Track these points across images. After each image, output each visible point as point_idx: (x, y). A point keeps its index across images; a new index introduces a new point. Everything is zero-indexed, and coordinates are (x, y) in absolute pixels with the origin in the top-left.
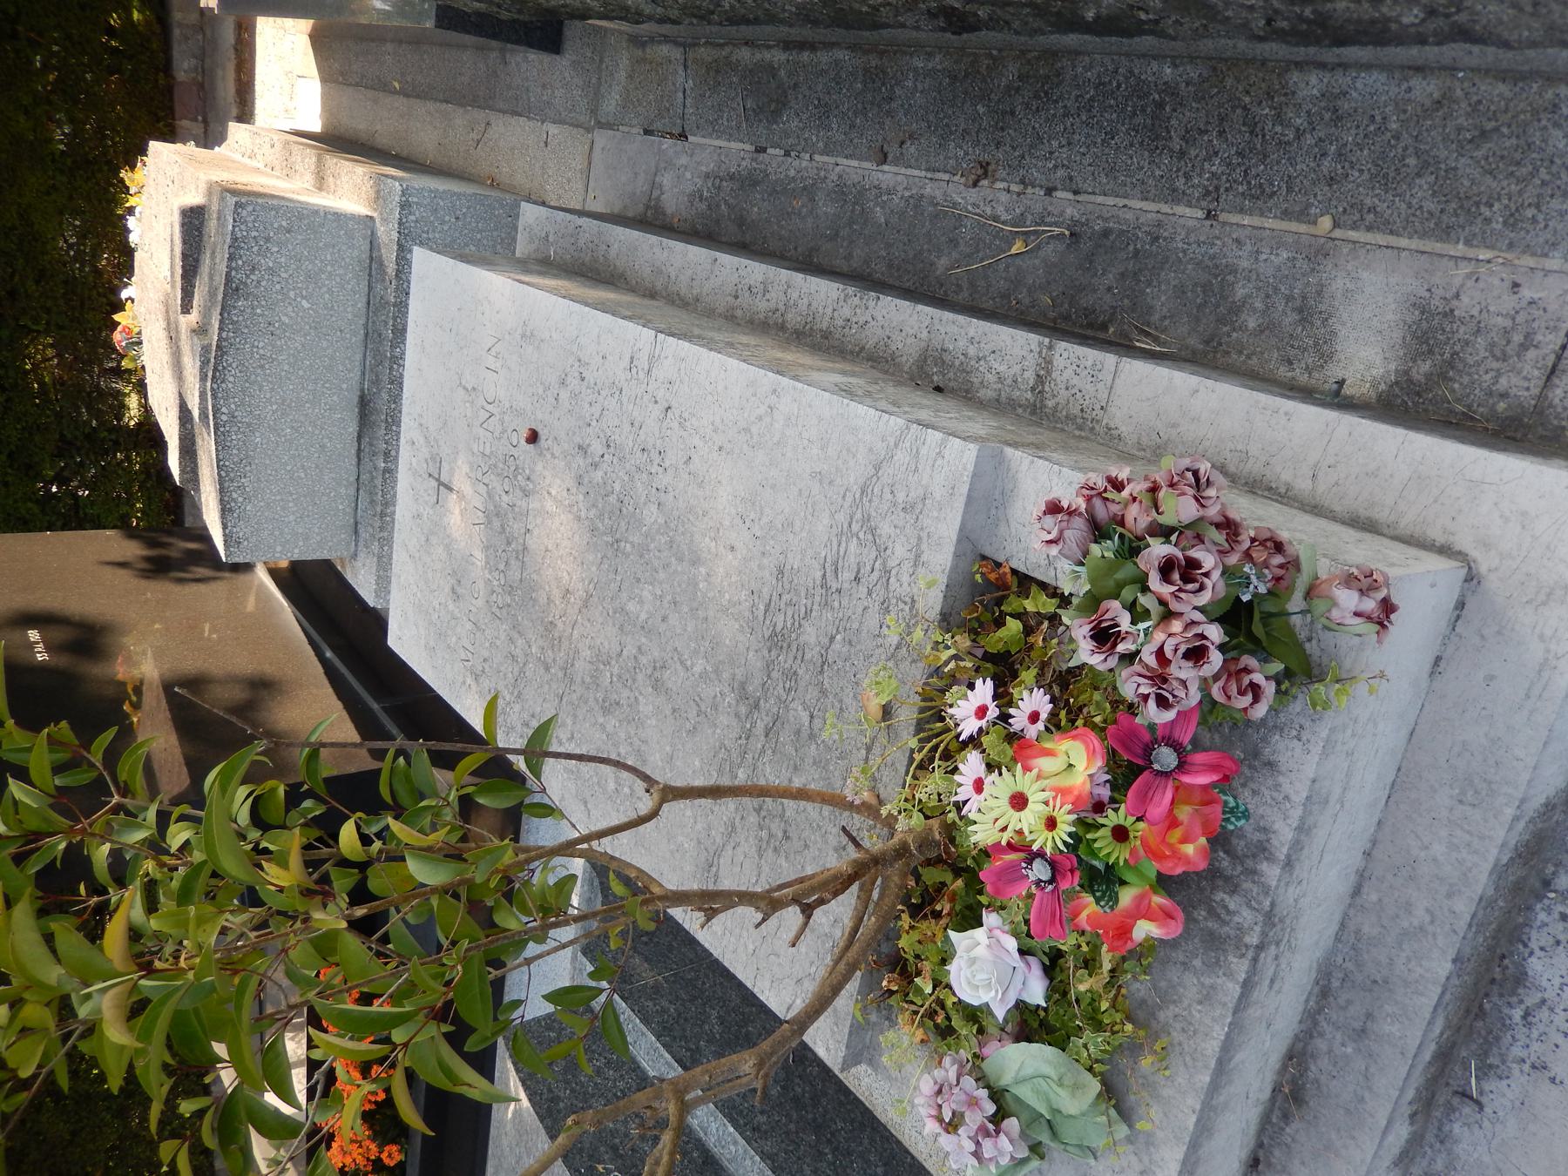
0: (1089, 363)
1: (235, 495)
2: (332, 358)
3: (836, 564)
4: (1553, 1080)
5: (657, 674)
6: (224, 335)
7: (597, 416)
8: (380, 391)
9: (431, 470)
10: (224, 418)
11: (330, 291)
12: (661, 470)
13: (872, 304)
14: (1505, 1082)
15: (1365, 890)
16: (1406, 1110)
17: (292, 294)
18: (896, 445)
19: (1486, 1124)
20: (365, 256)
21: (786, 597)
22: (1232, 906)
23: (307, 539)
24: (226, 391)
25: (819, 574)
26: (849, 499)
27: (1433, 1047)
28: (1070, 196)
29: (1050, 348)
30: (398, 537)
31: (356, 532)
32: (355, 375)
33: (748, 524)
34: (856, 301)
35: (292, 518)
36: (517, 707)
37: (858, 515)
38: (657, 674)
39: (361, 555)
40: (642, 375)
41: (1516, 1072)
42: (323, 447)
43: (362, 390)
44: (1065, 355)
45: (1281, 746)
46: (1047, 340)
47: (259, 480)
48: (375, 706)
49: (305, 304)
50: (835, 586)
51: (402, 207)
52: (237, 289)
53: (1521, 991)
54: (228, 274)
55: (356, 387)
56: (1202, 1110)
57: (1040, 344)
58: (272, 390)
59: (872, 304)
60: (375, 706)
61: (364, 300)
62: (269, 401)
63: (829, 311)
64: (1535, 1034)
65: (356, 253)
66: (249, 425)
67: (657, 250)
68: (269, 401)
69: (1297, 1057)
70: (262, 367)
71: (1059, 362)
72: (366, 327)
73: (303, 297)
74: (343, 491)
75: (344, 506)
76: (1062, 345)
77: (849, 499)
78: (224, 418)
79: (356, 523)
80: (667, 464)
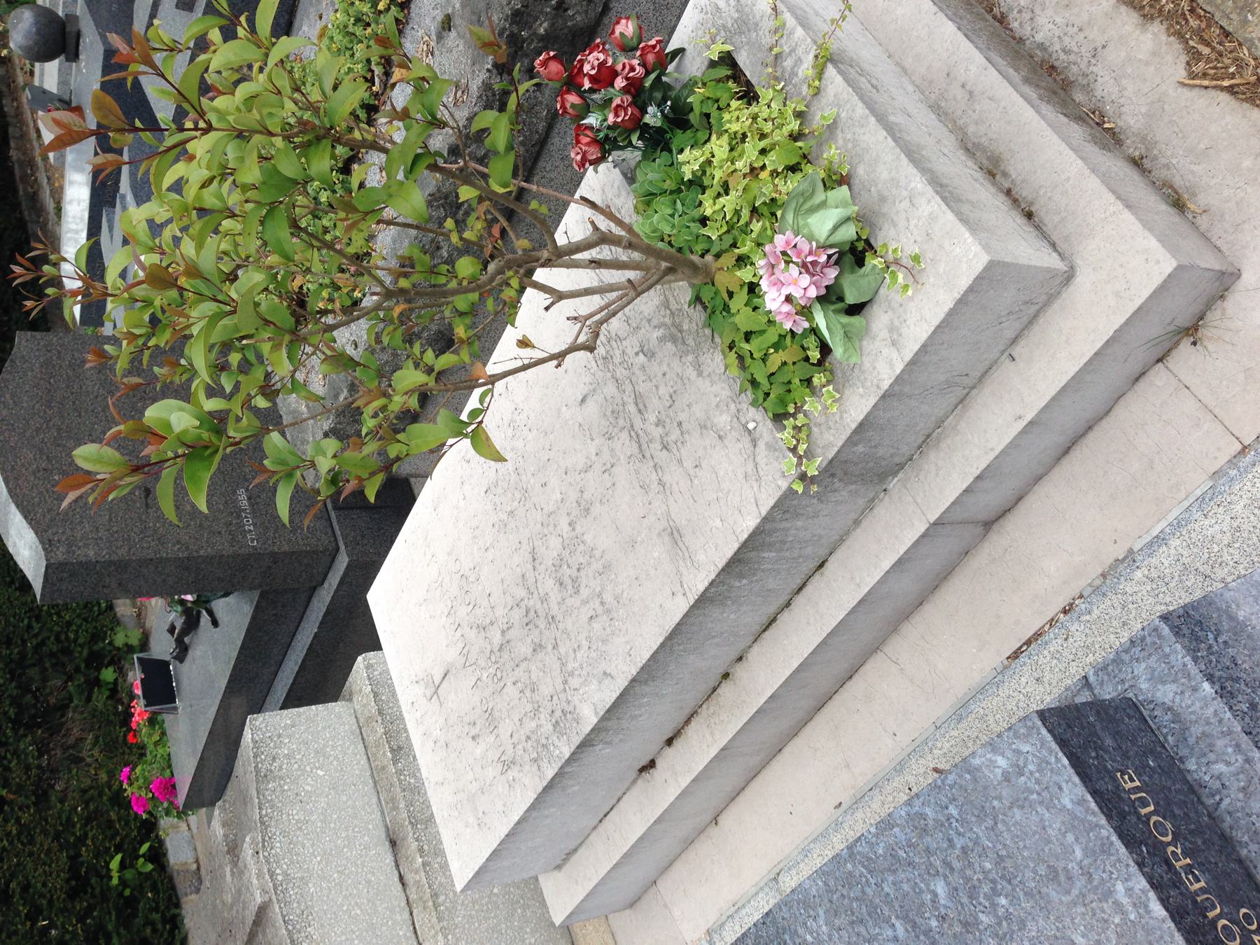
2: (354, 808)
4: (1104, 47)
10: (280, 878)
11: (336, 758)
14: (1099, 79)
17: (308, 769)
19: (1122, 101)
20: (355, 727)
24: (276, 855)
27: (1011, 71)
32: (377, 815)
41: (1095, 69)
42: (369, 882)
47: (322, 925)
49: (320, 773)
52: (266, 776)
53: (1050, 50)
54: (256, 767)
55: (381, 825)
58: (313, 845)
64: (1075, 49)
65: (347, 727)
66: (302, 878)
69: (970, 148)
70: (300, 829)
72: (373, 777)
74: (398, 917)
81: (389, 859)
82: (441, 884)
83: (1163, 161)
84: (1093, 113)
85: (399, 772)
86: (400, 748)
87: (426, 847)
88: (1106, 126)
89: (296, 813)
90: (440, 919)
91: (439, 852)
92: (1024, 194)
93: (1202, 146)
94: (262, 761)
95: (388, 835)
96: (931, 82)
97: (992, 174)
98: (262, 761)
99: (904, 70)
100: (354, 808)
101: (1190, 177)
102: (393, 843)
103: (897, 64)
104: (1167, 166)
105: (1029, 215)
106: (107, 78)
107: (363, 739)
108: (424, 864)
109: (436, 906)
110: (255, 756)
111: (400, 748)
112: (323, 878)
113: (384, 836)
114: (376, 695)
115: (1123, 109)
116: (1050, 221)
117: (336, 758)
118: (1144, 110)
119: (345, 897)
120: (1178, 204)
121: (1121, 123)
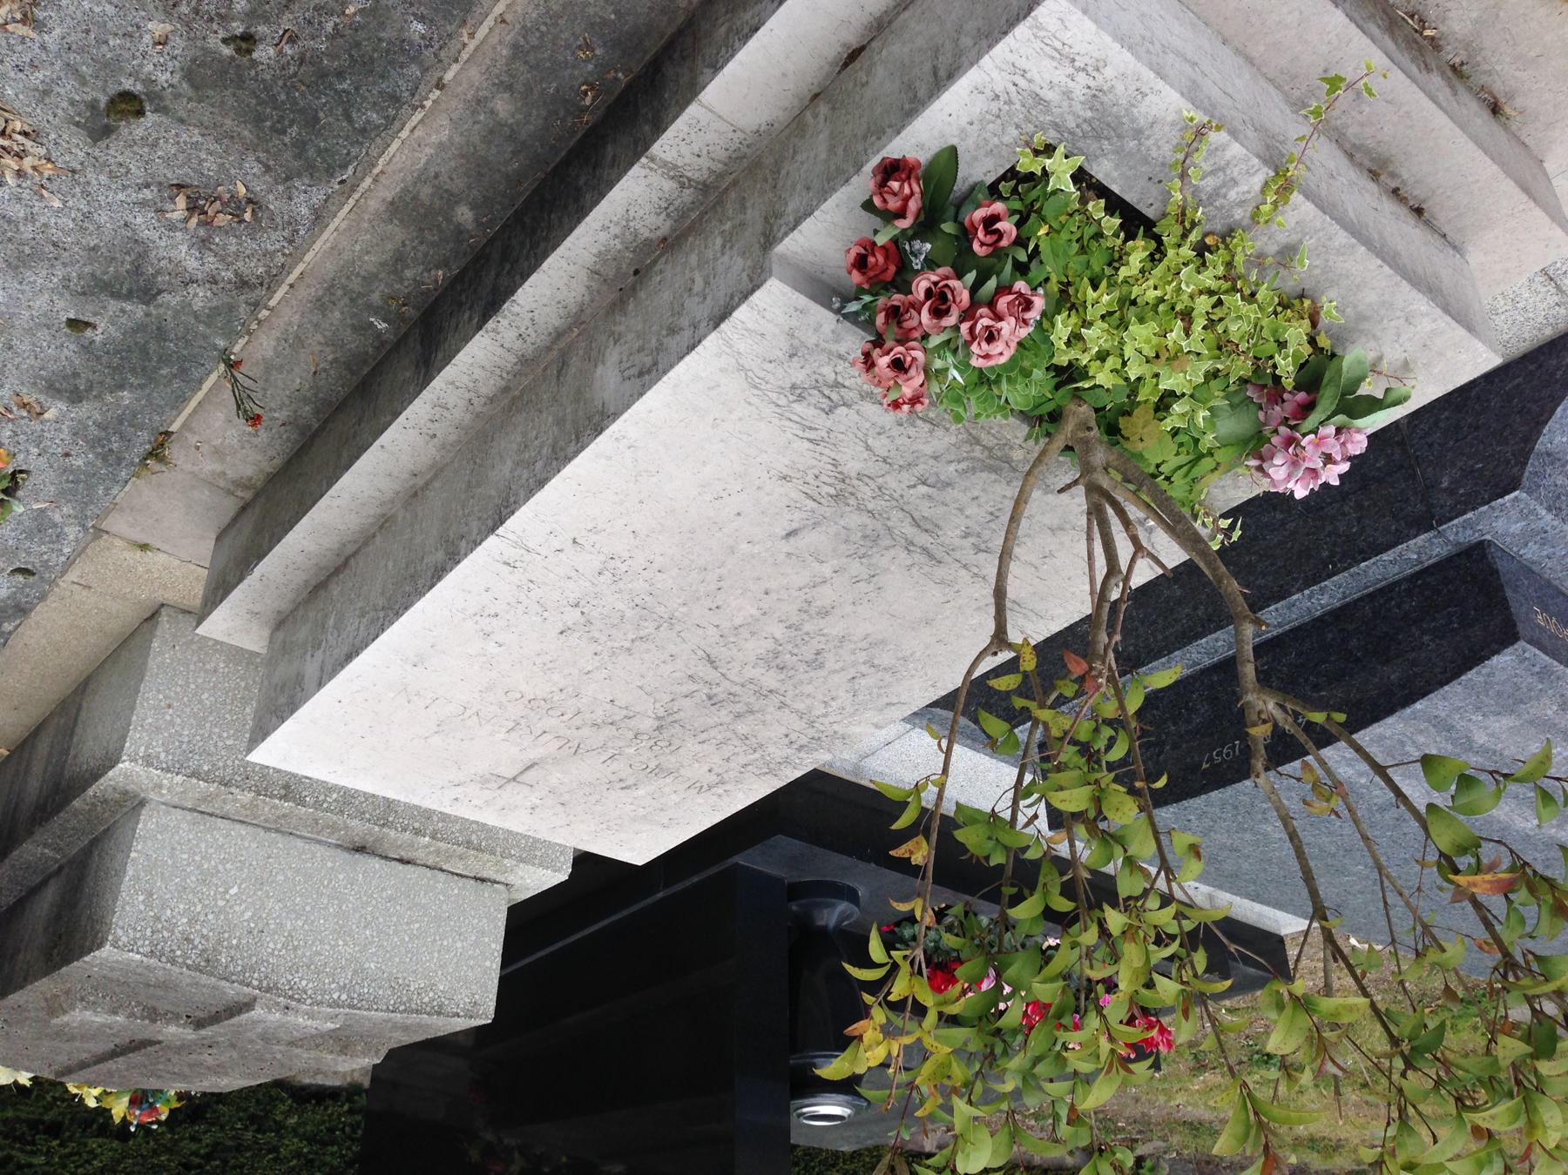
0: (686, 129)
1: (426, 1000)
2: (298, 871)
3: (805, 428)
5: (813, 611)
6: (255, 983)
7: (540, 610)
8: (346, 827)
9: (495, 786)
10: (344, 997)
11: (223, 861)
12: (629, 562)
13: (516, 309)
15: (1254, 54)
16: (1422, 77)
17: (221, 903)
18: (731, 347)
20: (189, 816)
21: (810, 479)
22: (1246, 188)
23: (483, 934)
25: (807, 444)
26: (753, 400)
28: (455, 67)
29: (652, 160)
30: (544, 834)
31: (483, 880)
32: (320, 851)
33: (725, 495)
34: (504, 322)
35: (459, 945)
36: (771, 749)
37: (774, 396)
38: (813, 611)
39: (511, 879)
40: (527, 557)
43: (338, 846)
44: (666, 148)
45: (1143, 109)
46: (643, 160)
48: (660, 895)
49: (234, 891)
50: (824, 434)
51: (149, 764)
52: (208, 961)
55: (332, 852)
56: (1384, 260)
57: (643, 167)
59: (516, 309)
60: (660, 895)
61: (238, 826)
62: (333, 947)
63: (500, 351)
65: (184, 826)
66: (355, 972)
67: (337, 502)
68: (333, 947)
70: (295, 948)
71: (668, 157)
72: (268, 830)
73: (226, 892)
74: (440, 886)
75: (456, 886)
76: (656, 149)
77: (753, 400)
78: (344, 997)
79: (476, 879)
80: (626, 555)
81: (376, 863)
82: (460, 831)
83: (1486, 67)
84: (1412, 17)
85: (317, 805)
86: (286, 787)
87: (417, 825)
88: (1428, 33)
89: (272, 944)
90: (493, 853)
91: (428, 814)
92: (1416, 193)
93: (1533, 54)
94: (185, 956)
95: (347, 849)
96: (1294, 77)
97: (1374, 175)
98: (185, 956)
99: (1250, 61)
100: (298, 871)
101: (1512, 82)
102: (360, 849)
103: (1238, 52)
104: (1489, 73)
105: (1419, 211)
106: (509, 970)
107: (211, 815)
108: (433, 837)
109: (478, 849)
110: (173, 961)
111: (286, 787)
112: (364, 949)
113: (346, 855)
114: (195, 774)
115: (1450, 14)
116: (1442, 218)
117: (223, 861)
118: (1474, 15)
119: (396, 932)
120: (1495, 109)
121: (1443, 28)
